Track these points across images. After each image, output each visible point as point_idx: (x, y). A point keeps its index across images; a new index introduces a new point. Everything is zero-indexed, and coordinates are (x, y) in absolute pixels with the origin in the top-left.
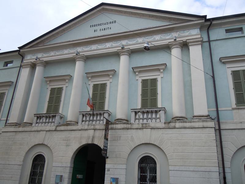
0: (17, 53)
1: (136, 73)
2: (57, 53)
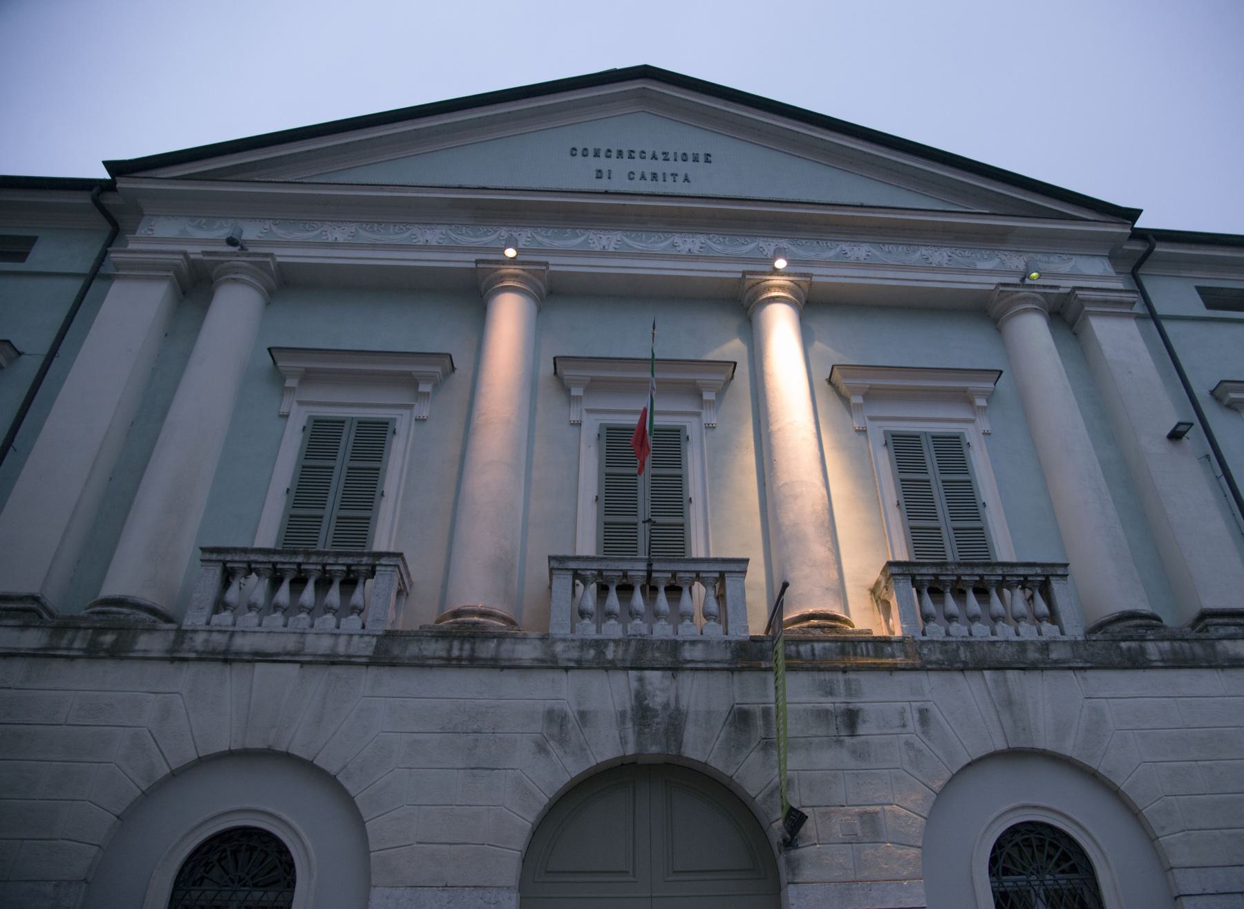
0: (84, 199)
1: (417, 385)
2: (366, 236)
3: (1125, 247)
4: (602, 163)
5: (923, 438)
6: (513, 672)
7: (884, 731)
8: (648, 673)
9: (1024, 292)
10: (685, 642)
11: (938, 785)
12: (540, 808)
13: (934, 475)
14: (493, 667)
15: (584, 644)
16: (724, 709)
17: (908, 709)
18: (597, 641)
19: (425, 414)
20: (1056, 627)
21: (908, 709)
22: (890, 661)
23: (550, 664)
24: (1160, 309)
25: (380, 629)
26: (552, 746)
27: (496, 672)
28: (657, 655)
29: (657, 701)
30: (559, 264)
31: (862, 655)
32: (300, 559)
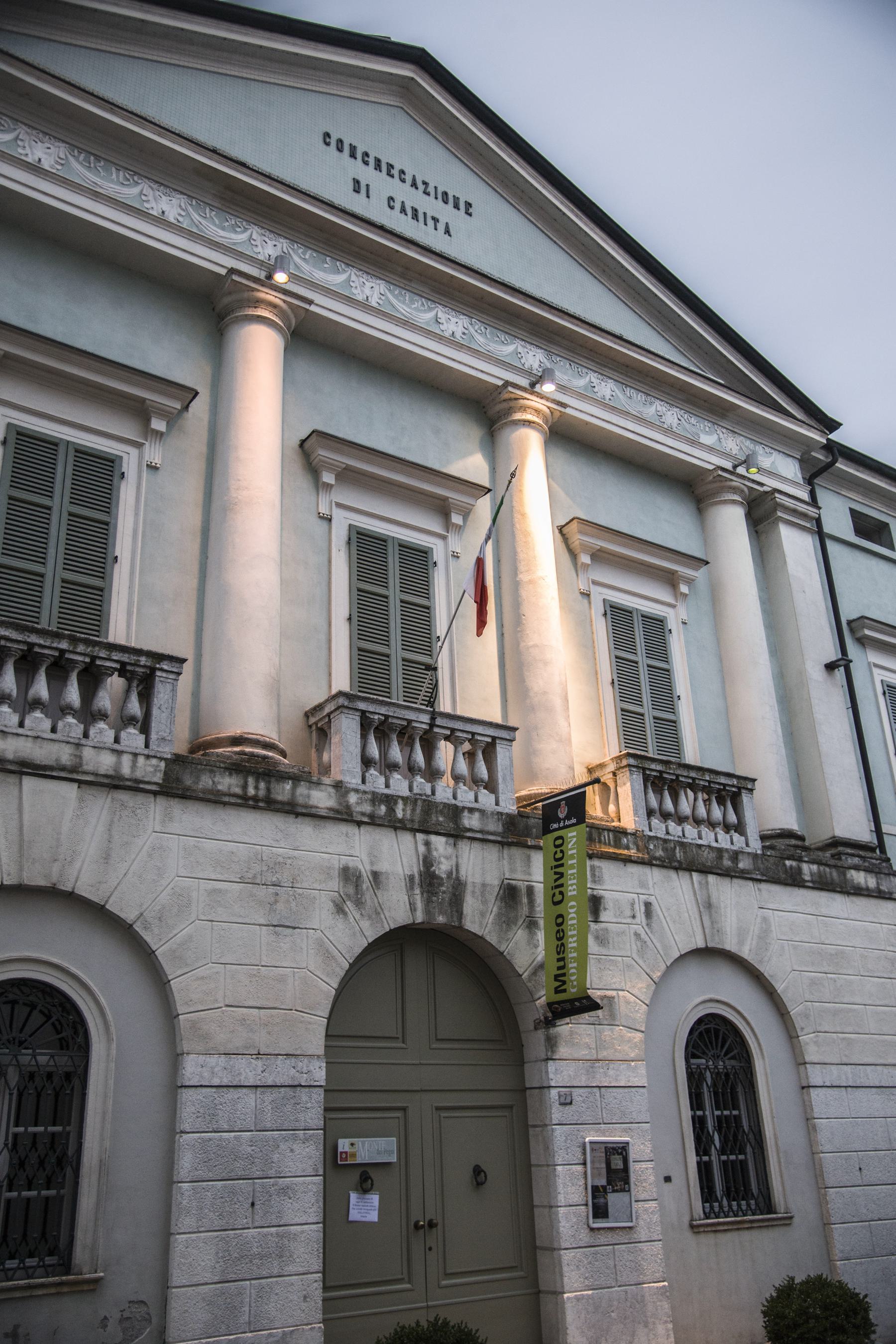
3: (813, 454)
4: (367, 174)
5: (62, 450)
6: (307, 819)
7: (619, 920)
8: (434, 838)
9: (737, 482)
10: (464, 808)
11: (657, 975)
12: (342, 974)
13: (60, 503)
14: (288, 812)
15: (376, 798)
16: (496, 882)
17: (637, 901)
18: (387, 796)
19: (157, 461)
20: (743, 838)
21: (637, 901)
22: (625, 852)
23: (343, 816)
24: (827, 529)
25: (167, 751)
26: (349, 906)
27: (291, 819)
28: (441, 819)
29: (443, 868)
30: (326, 307)
31: (605, 844)
32: (64, 645)
